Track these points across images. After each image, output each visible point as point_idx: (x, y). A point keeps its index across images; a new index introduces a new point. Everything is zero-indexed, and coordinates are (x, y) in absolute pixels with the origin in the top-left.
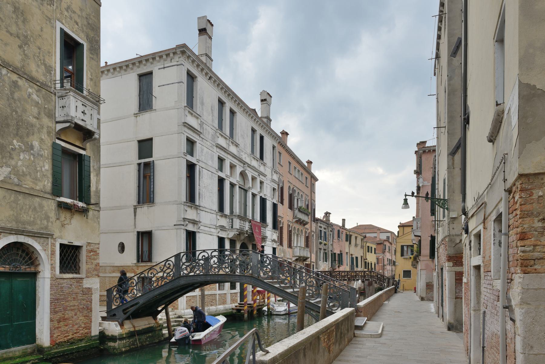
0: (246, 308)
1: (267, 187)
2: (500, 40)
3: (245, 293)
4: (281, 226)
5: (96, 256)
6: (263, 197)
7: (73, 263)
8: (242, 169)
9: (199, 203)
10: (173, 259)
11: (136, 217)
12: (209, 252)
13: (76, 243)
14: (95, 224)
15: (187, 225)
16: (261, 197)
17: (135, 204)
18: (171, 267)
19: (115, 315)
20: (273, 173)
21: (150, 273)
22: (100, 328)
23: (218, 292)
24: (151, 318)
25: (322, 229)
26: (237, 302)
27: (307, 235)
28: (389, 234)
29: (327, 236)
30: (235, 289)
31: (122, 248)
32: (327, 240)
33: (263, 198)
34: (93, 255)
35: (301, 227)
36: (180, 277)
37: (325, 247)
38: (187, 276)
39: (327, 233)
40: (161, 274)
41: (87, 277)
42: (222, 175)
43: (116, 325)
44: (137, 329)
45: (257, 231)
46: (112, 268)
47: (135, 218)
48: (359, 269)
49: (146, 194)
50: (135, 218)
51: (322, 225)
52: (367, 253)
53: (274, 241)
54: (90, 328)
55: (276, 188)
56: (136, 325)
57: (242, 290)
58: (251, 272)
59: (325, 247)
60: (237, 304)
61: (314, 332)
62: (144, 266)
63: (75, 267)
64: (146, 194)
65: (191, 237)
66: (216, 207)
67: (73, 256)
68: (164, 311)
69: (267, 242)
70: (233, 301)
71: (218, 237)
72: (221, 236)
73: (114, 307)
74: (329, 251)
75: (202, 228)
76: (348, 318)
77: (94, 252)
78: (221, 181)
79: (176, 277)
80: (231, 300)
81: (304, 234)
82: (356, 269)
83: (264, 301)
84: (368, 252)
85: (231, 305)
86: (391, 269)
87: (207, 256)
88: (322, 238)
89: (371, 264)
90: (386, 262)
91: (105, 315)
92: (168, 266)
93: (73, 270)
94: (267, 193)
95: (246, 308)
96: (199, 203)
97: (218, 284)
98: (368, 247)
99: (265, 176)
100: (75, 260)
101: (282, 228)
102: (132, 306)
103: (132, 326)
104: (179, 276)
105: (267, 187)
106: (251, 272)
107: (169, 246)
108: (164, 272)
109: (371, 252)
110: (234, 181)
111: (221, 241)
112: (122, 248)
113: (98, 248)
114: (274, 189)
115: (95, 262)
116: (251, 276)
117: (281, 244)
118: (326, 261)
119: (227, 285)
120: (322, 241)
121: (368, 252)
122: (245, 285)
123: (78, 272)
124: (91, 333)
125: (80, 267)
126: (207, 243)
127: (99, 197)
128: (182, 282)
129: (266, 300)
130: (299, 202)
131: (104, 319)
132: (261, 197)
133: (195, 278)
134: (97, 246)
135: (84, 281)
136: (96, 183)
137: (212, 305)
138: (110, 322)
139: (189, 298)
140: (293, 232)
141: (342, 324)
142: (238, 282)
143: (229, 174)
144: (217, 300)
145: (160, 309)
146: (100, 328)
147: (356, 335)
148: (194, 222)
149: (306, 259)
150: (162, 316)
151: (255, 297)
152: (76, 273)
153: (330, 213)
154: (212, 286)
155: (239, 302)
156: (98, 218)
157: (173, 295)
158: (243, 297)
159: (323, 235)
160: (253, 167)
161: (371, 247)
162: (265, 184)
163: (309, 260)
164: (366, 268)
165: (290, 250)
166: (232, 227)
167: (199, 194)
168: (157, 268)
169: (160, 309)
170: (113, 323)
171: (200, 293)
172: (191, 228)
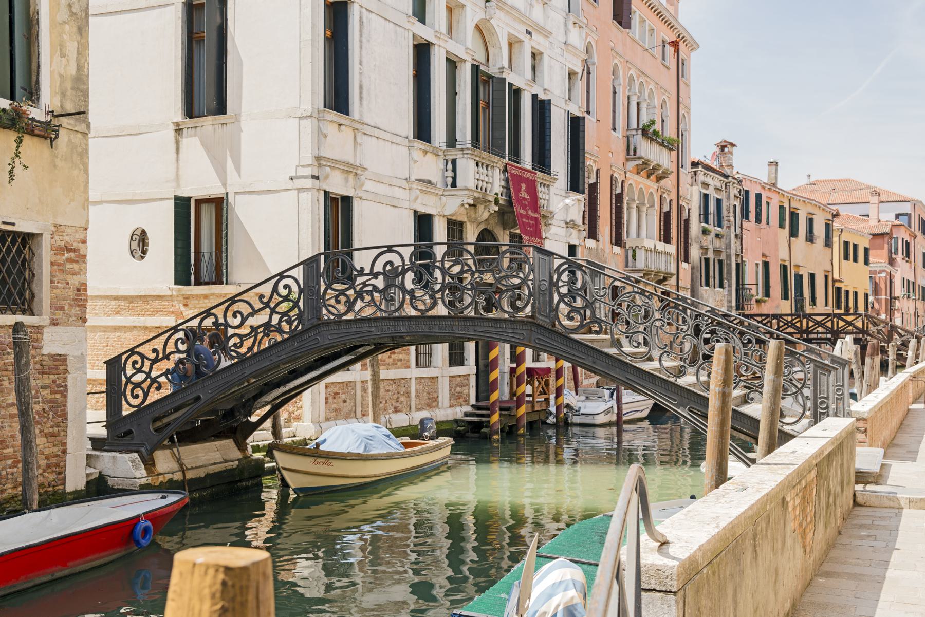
0: (496, 418)
1: (551, 67)
2: (361, 87)
3: (493, 376)
4: (592, 180)
5: (77, 262)
6: (542, 96)
7: (15, 283)
8: (480, 15)
9: (361, 114)
10: (298, 273)
11: (181, 155)
12: (219, 312)
13: (23, 226)
14: (76, 172)
15: (327, 177)
16: (535, 96)
17: (179, 117)
18: (294, 296)
19: (129, 433)
20: (570, 25)
21: (230, 314)
22: (90, 470)
23: (414, 372)
24: (229, 443)
25: (711, 191)
26: (467, 401)
27: (666, 208)
28: (906, 208)
29: (725, 213)
30: (462, 364)
31: (141, 242)
32: (725, 224)
33: (542, 101)
34: (70, 260)
35: (651, 185)
36: (319, 324)
37: (718, 243)
38: (338, 321)
39: (725, 204)
40: (261, 319)
41: (54, 323)
42: (425, 33)
43: (133, 461)
44: (190, 475)
45: (524, 195)
46: (113, 303)
47: (177, 160)
48: (820, 308)
49: (206, 87)
50: (177, 160)
51: (708, 180)
52: (844, 262)
53: (570, 225)
54: (61, 473)
55: (579, 70)
56: (188, 463)
57: (485, 367)
58: (529, 309)
59: (718, 243)
60: (469, 409)
61: (774, 484)
62: (206, 297)
63: (21, 294)
64: (206, 87)
65: (338, 212)
66: (407, 125)
67: (14, 262)
68: (268, 423)
69: (553, 229)
70: (457, 397)
71: (415, 212)
72: (423, 210)
73: (126, 411)
74: (729, 257)
75: (369, 186)
76: (841, 448)
77: (73, 254)
78: (422, 51)
79: (308, 325)
80: (451, 395)
81: (657, 206)
82: (808, 309)
83: (547, 400)
84: (846, 258)
85: (450, 411)
86: (912, 311)
87: (398, 262)
88: (711, 218)
89: (856, 294)
90: (899, 291)
91: (101, 431)
92: (284, 292)
93: (14, 303)
94: (552, 86)
95: (496, 418)
96: (361, 114)
97: (413, 348)
98: (846, 244)
99: (547, 34)
100: (21, 273)
101: (594, 188)
102: (177, 409)
103: (176, 466)
104: (315, 321)
105: (551, 67)
106: (529, 309)
107: (275, 239)
108: (273, 311)
109: (855, 260)
110: (458, 51)
111: (423, 223)
112: (141, 242)
113: (84, 242)
114: (571, 75)
115: (74, 281)
116: (531, 322)
117: (593, 234)
118: (721, 286)
119: (441, 351)
120: (710, 227)
121: (846, 258)
122: (520, 349)
123: (29, 311)
124: (64, 484)
125: (33, 296)
126: (382, 228)
127: (86, 94)
128: (326, 339)
129: (552, 397)
130: (644, 111)
131: (97, 443)
132: (535, 96)
133: (365, 328)
134: (79, 236)
135: (46, 336)
136: (79, 53)
137: (396, 410)
138: (117, 454)
139: (332, 390)
140: (626, 199)
141: (829, 465)
142: (470, 340)
143: (444, 29)
144: (413, 394)
145: (254, 419)
146: (90, 470)
147: (860, 499)
148: (351, 170)
149: (665, 279)
150: (262, 436)
151: (520, 390)
152: (24, 312)
153: (733, 145)
154: (399, 353)
155: (473, 401)
156: (84, 154)
157: (296, 378)
158: (485, 386)
159: (712, 207)
160: (512, 7)
161: (855, 246)
162: (546, 58)
163: (673, 281)
164: (838, 307)
165: (617, 249)
166: (454, 185)
167: (361, 87)
168: (251, 297)
169: (254, 419)
170: (127, 456)
171: (367, 375)
172: (338, 186)
